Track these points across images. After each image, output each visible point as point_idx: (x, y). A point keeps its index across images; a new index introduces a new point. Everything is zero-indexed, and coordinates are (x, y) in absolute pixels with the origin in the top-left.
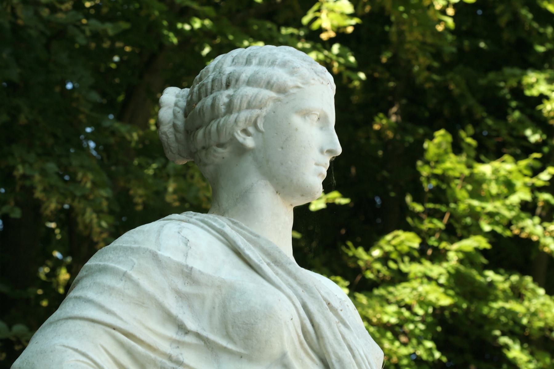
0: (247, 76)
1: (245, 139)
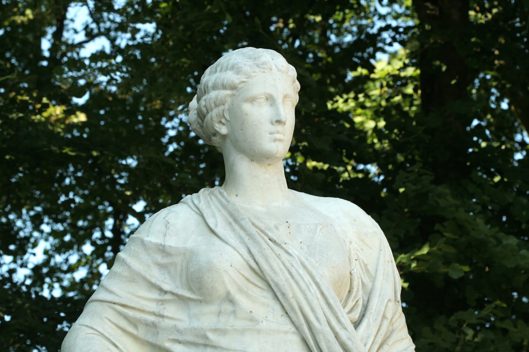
0: (212, 83)
1: (220, 129)
